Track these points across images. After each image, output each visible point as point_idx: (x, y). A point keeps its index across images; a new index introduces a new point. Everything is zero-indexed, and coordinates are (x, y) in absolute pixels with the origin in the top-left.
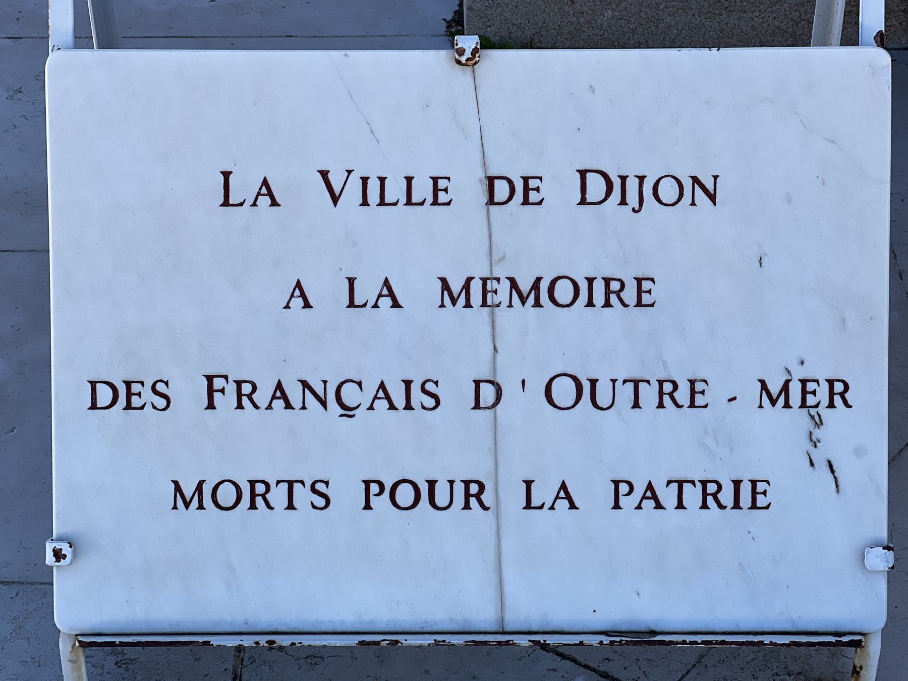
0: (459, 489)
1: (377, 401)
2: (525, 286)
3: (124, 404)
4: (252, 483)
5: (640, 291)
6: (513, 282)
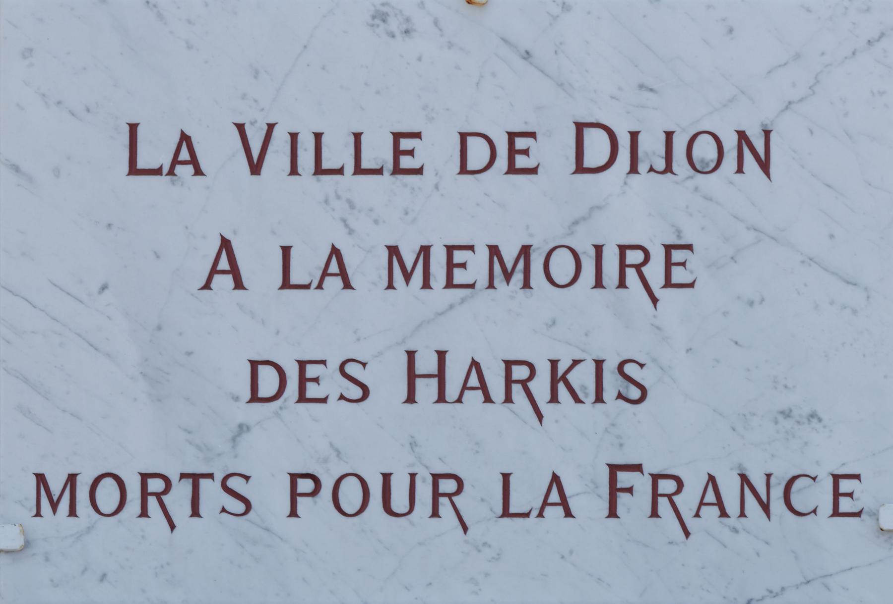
0: (424, 492)
1: (467, 392)
2: (509, 254)
3: (505, 167)
4: (145, 477)
5: (669, 264)
6: (494, 251)
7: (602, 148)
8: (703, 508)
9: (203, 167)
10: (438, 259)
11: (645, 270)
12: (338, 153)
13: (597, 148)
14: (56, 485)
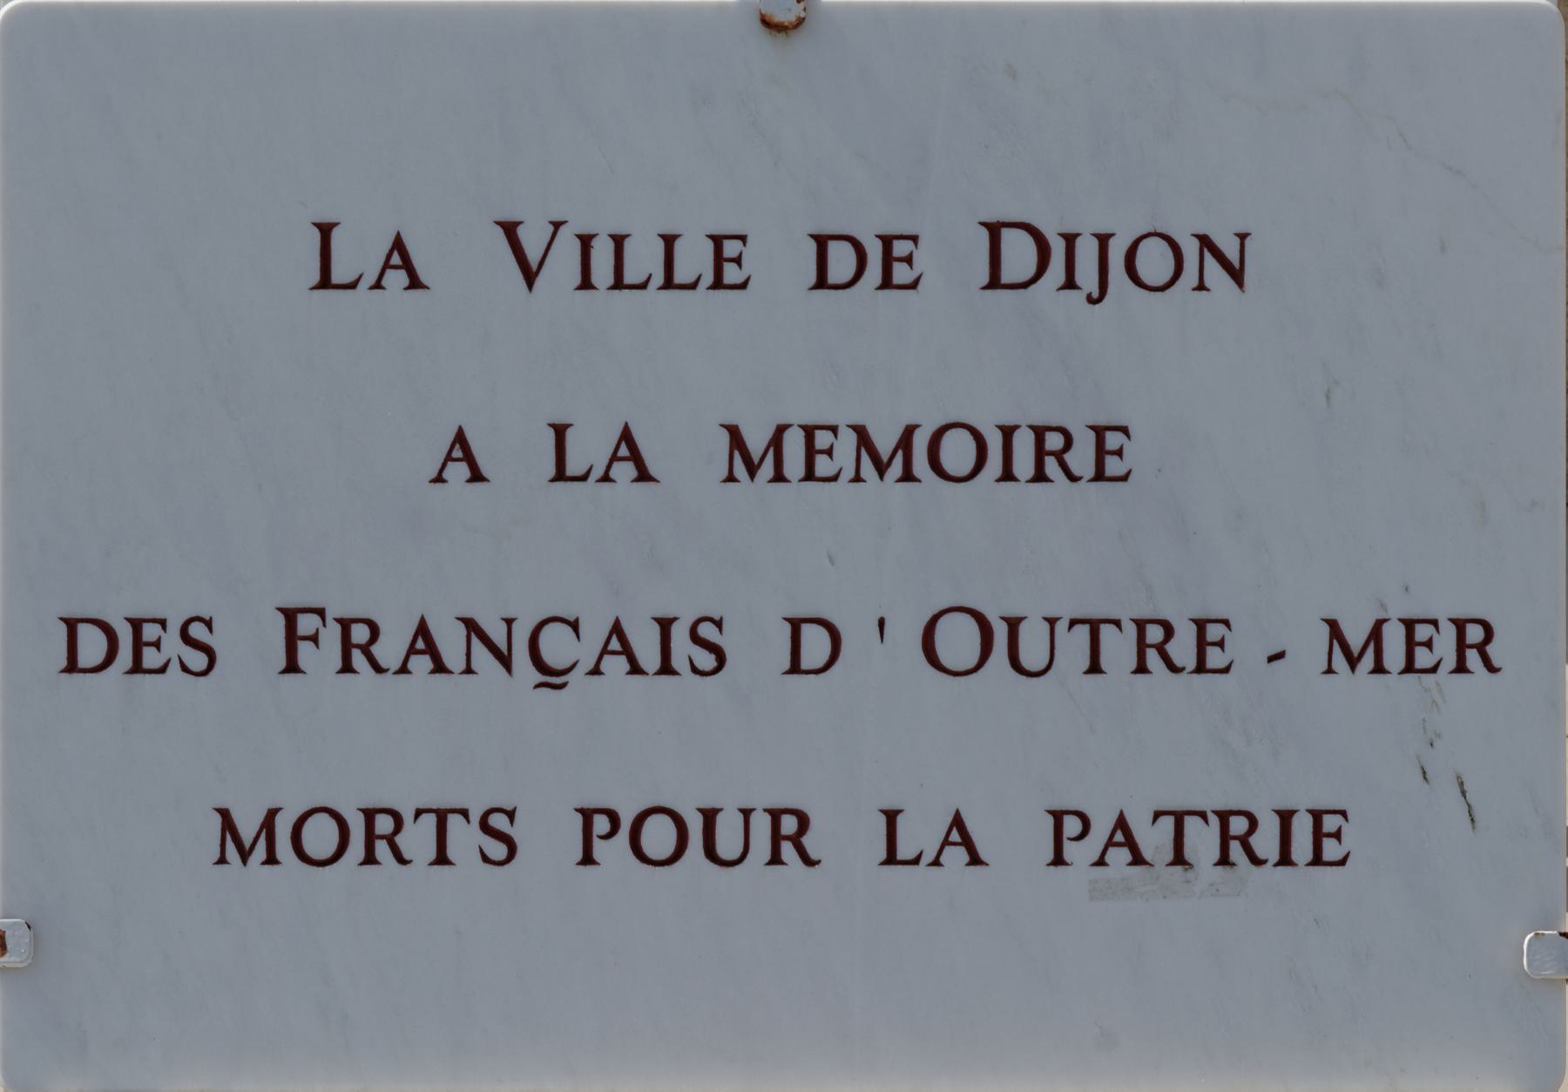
1: (606, 657)
6: (862, 434)
7: (1031, 256)
8: (1111, 850)
9: (424, 276)
10: (1394, 639)
11: (1490, 649)
12: (644, 259)
13: (1019, 255)
14: (248, 827)
